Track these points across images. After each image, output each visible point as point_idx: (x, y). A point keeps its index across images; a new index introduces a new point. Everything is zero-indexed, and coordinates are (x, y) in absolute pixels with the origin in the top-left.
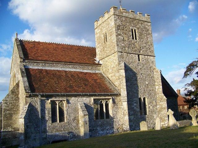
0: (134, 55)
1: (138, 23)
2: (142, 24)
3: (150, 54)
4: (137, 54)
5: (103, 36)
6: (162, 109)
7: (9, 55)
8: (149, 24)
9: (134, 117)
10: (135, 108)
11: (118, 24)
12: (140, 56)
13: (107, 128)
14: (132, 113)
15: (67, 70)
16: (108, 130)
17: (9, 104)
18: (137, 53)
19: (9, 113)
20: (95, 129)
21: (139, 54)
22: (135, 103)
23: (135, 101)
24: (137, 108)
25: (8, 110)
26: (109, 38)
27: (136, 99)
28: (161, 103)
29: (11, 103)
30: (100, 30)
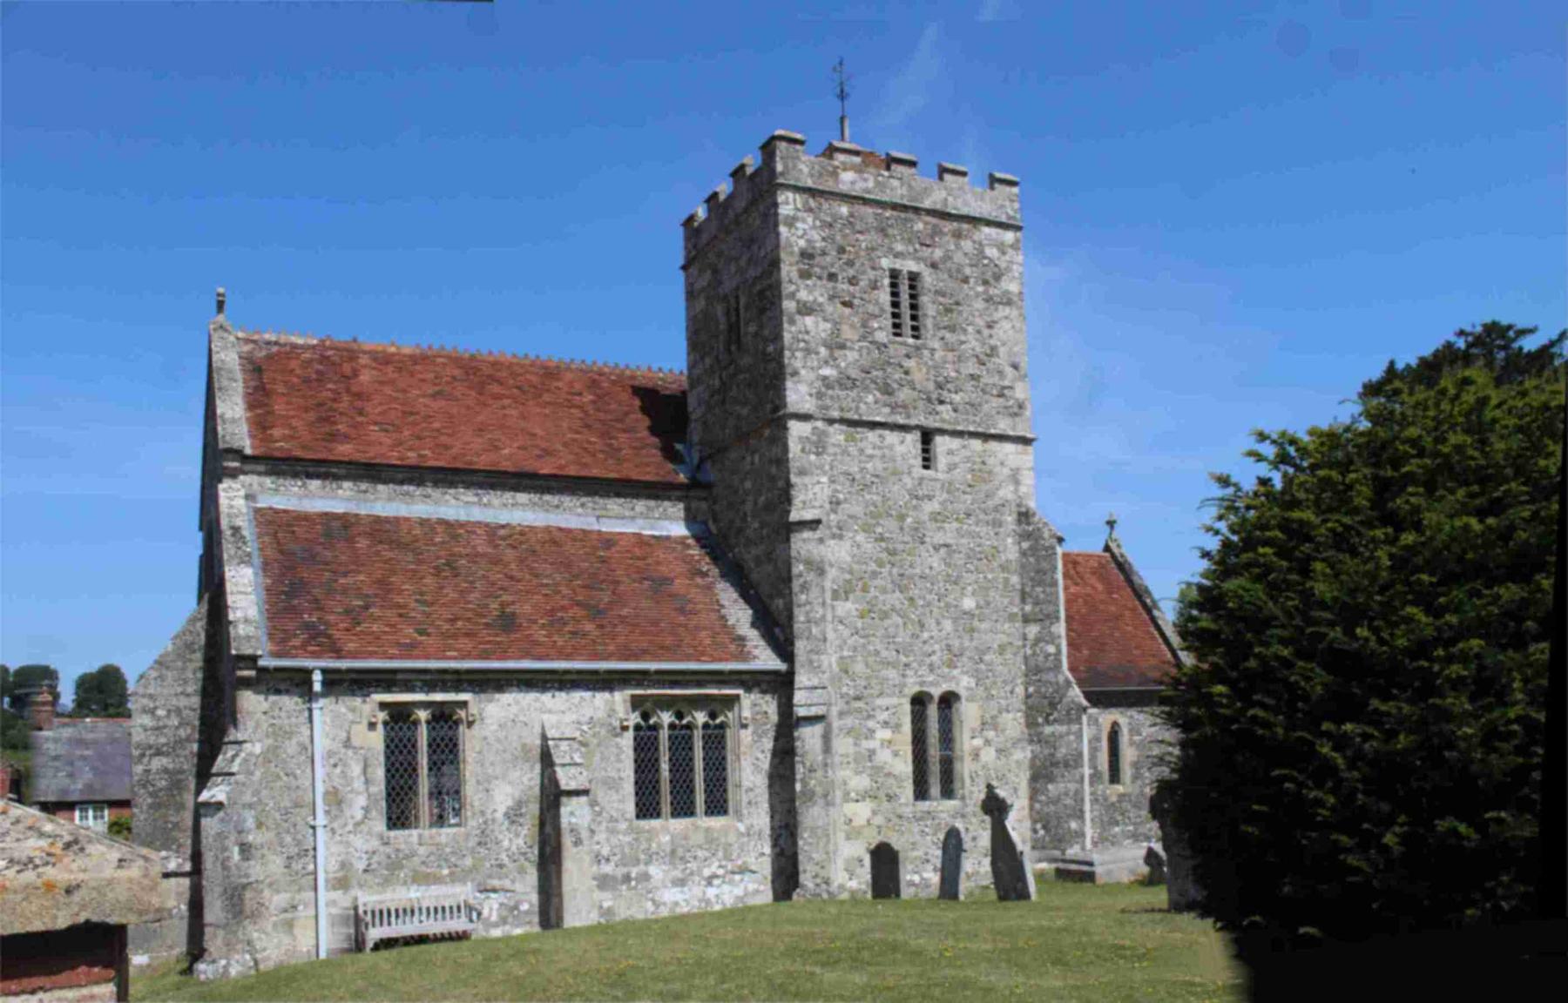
0: (891, 437)
1: (936, 232)
2: (958, 235)
3: (1003, 425)
4: (917, 427)
5: (719, 310)
6: (1052, 764)
7: (911, 884)
8: (1009, 236)
9: (874, 813)
10: (884, 756)
11: (802, 243)
12: (942, 444)
13: (707, 872)
14: (336, 524)
15: (504, 517)
16: (710, 884)
17: (168, 716)
18: (913, 422)
19: (166, 771)
20: (634, 872)
21: (931, 423)
22: (886, 724)
23: (884, 716)
24: (896, 754)
25: (159, 753)
26: (752, 328)
27: (895, 701)
28: (1048, 730)
29: (178, 711)
30: (708, 275)
